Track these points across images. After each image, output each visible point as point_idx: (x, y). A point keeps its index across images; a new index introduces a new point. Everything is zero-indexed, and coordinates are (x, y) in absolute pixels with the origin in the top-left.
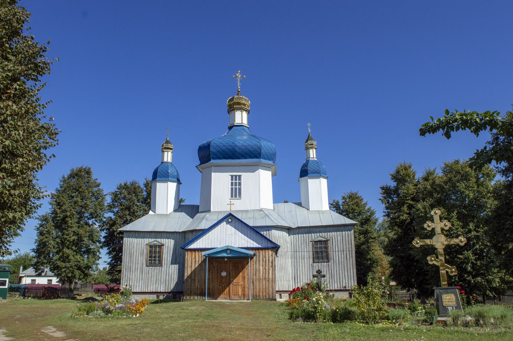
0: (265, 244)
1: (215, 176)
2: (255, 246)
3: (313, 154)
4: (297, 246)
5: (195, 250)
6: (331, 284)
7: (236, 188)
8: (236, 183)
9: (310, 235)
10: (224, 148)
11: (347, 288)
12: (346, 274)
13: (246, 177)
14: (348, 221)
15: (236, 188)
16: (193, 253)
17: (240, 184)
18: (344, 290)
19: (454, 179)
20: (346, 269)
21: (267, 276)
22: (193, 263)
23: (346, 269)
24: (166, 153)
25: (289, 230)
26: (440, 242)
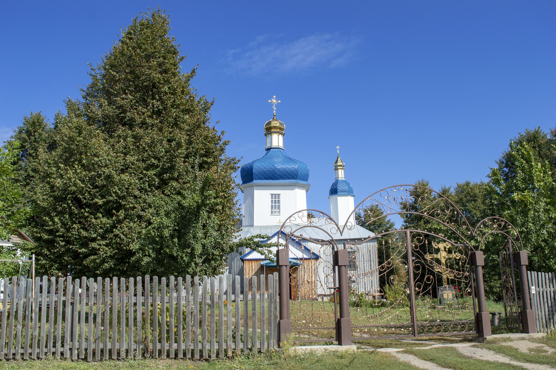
3: (341, 174)
5: (249, 260)
10: (265, 170)
14: (372, 235)
16: (250, 262)
17: (279, 201)
19: (465, 200)
22: (251, 271)
26: (443, 256)
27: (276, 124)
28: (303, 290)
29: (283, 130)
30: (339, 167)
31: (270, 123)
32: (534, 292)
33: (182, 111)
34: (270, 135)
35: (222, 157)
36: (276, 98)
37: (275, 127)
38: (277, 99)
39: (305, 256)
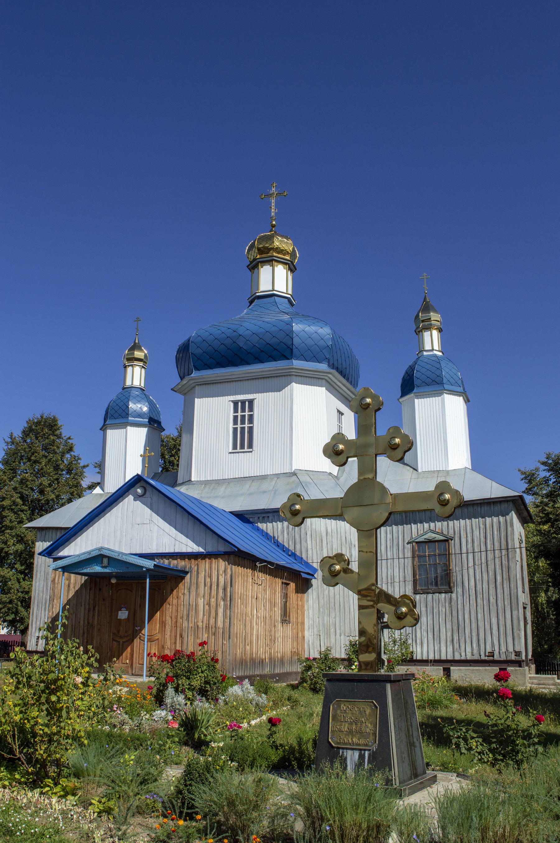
0: (213, 546)
2: (190, 550)
3: (432, 341)
6: (456, 646)
7: (243, 429)
9: (407, 527)
11: (496, 657)
12: (494, 621)
13: (264, 402)
15: (243, 429)
17: (251, 418)
18: (489, 662)
20: (493, 608)
21: (212, 621)
23: (493, 608)
24: (129, 370)
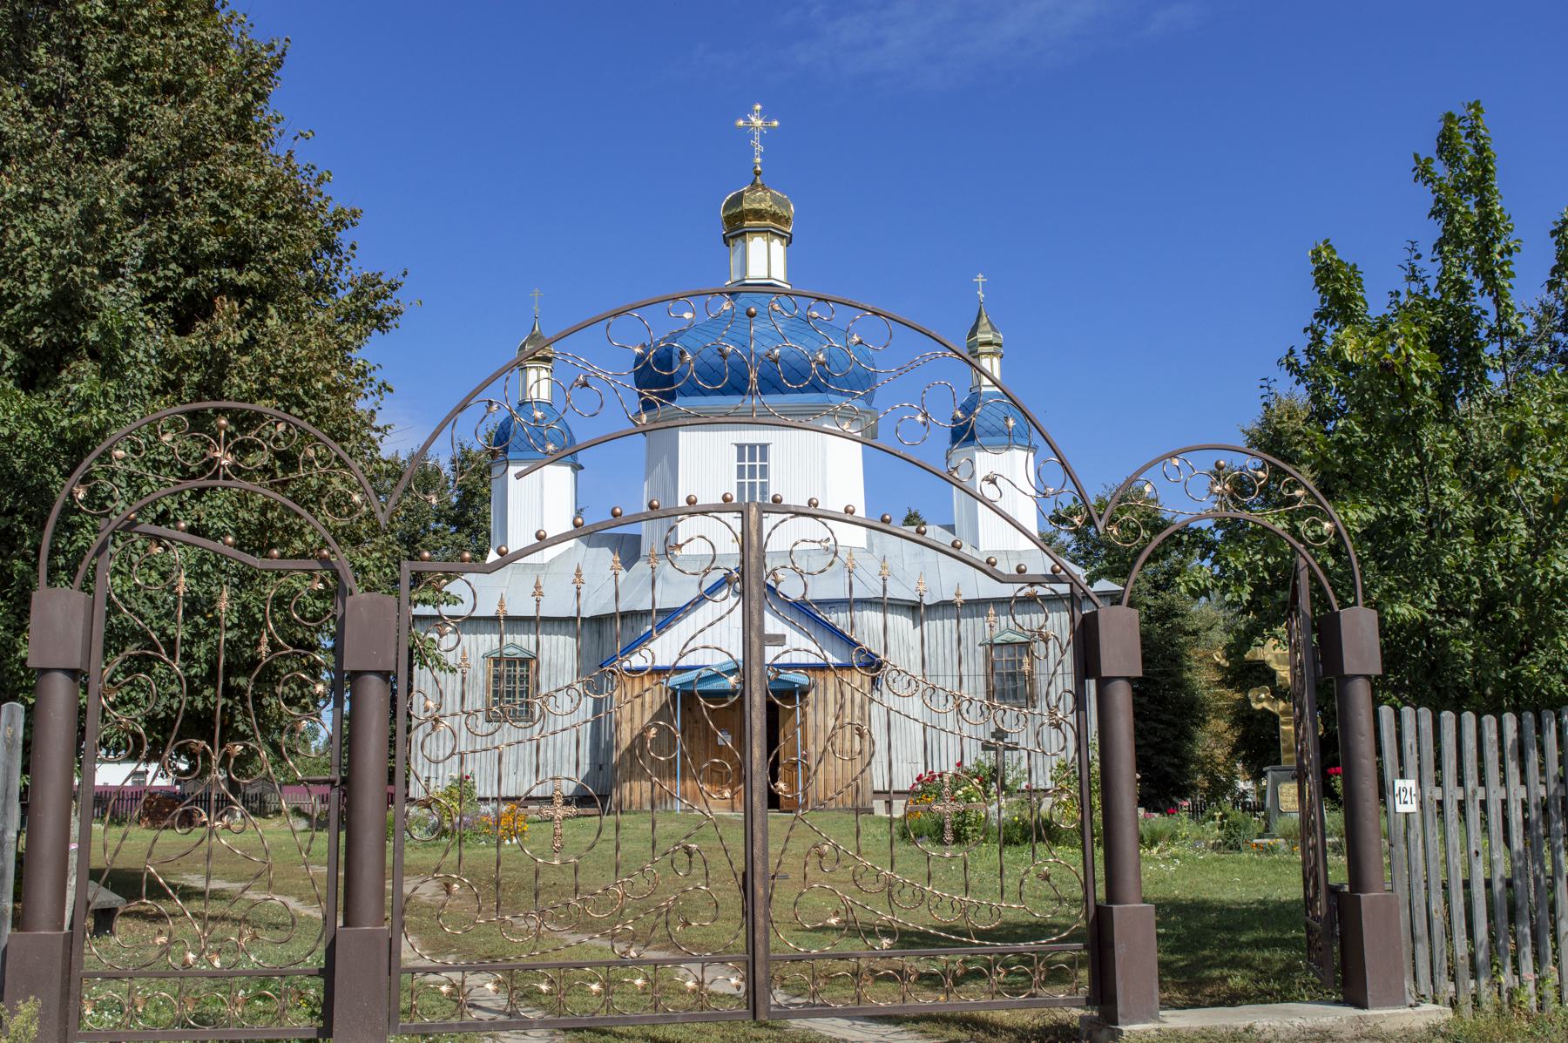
1: (689, 441)
4: (940, 660)
7: (752, 485)
8: (752, 468)
15: (752, 485)
25: (914, 610)
27: (761, 200)
28: (829, 776)
29: (787, 221)
30: (981, 349)
31: (739, 199)
32: (1412, 807)
33: (151, 91)
34: (739, 241)
35: (344, 278)
36: (762, 113)
37: (759, 214)
38: (766, 114)
39: (833, 660)
